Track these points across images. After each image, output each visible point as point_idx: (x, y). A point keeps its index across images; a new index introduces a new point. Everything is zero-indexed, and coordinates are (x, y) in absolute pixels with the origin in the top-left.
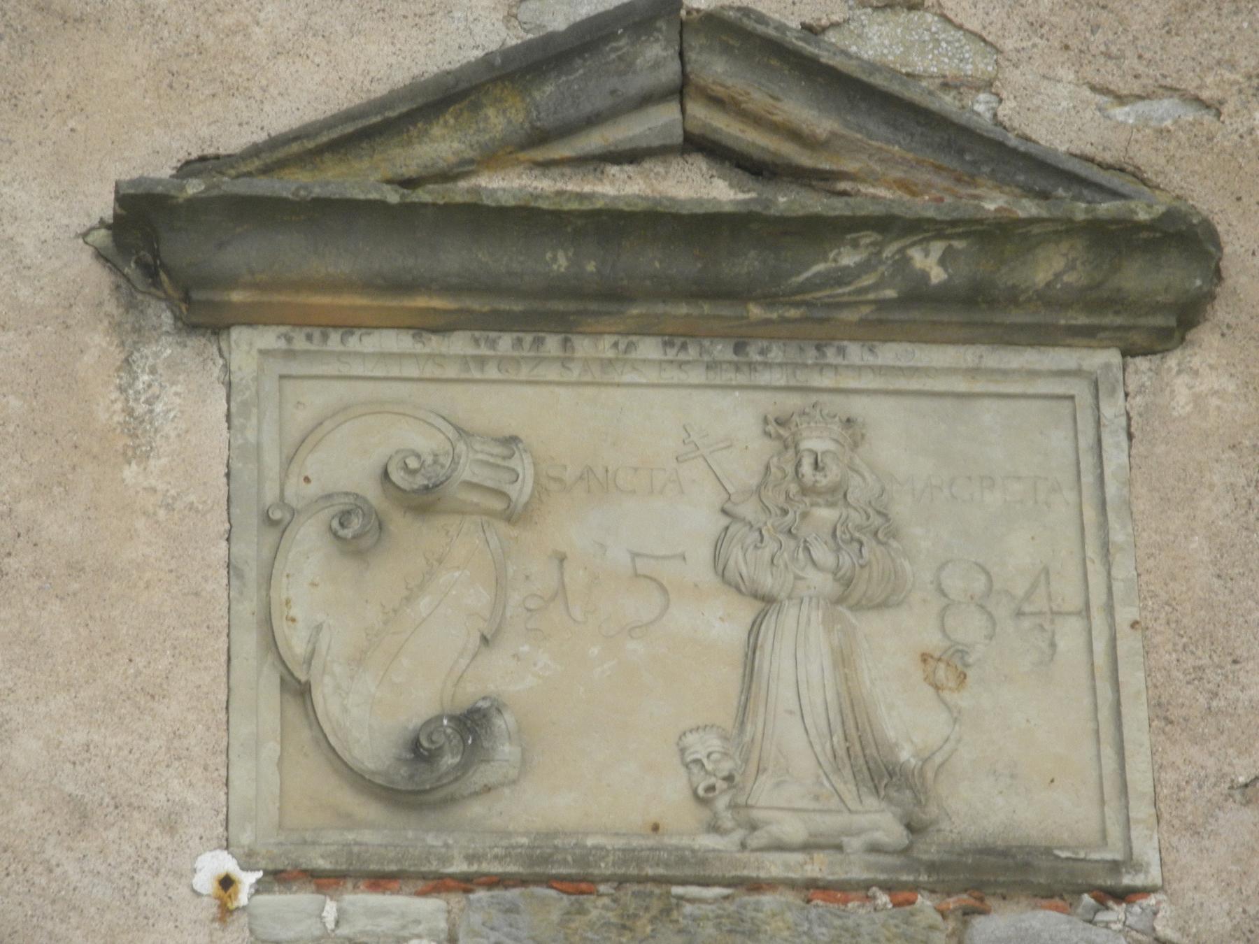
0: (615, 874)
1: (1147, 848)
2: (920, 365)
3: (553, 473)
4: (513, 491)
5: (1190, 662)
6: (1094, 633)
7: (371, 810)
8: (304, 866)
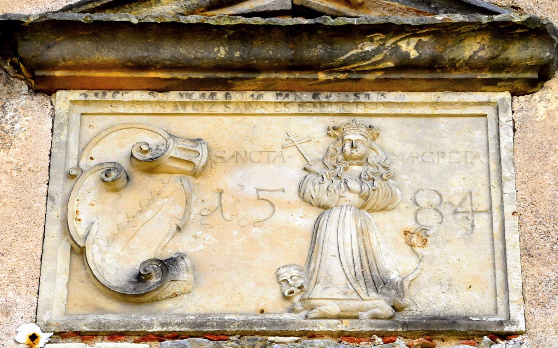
0: (238, 331)
1: (517, 314)
2: (407, 101)
3: (218, 155)
4: (196, 161)
5: (543, 228)
6: (494, 219)
7: (114, 306)
8: (75, 330)
